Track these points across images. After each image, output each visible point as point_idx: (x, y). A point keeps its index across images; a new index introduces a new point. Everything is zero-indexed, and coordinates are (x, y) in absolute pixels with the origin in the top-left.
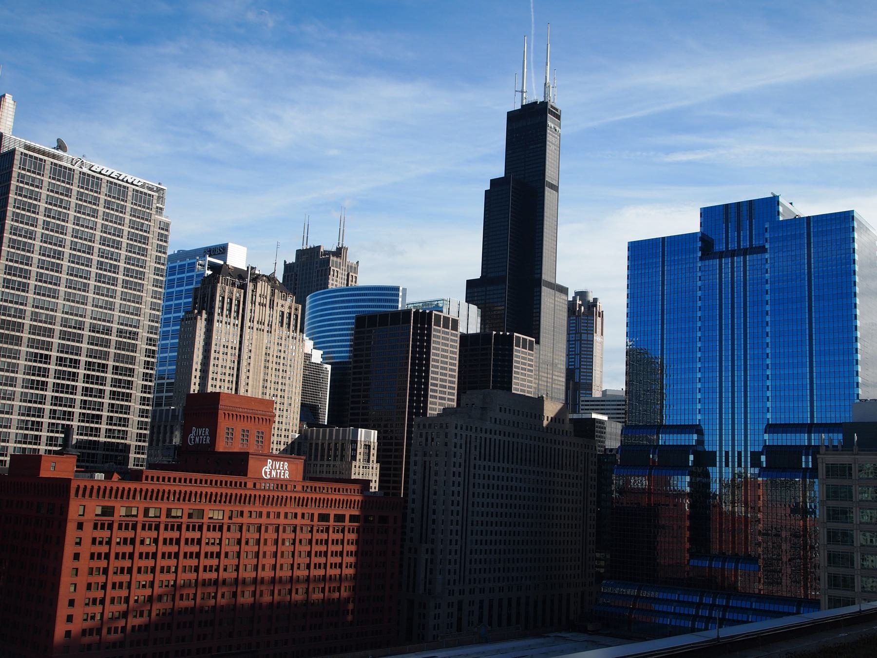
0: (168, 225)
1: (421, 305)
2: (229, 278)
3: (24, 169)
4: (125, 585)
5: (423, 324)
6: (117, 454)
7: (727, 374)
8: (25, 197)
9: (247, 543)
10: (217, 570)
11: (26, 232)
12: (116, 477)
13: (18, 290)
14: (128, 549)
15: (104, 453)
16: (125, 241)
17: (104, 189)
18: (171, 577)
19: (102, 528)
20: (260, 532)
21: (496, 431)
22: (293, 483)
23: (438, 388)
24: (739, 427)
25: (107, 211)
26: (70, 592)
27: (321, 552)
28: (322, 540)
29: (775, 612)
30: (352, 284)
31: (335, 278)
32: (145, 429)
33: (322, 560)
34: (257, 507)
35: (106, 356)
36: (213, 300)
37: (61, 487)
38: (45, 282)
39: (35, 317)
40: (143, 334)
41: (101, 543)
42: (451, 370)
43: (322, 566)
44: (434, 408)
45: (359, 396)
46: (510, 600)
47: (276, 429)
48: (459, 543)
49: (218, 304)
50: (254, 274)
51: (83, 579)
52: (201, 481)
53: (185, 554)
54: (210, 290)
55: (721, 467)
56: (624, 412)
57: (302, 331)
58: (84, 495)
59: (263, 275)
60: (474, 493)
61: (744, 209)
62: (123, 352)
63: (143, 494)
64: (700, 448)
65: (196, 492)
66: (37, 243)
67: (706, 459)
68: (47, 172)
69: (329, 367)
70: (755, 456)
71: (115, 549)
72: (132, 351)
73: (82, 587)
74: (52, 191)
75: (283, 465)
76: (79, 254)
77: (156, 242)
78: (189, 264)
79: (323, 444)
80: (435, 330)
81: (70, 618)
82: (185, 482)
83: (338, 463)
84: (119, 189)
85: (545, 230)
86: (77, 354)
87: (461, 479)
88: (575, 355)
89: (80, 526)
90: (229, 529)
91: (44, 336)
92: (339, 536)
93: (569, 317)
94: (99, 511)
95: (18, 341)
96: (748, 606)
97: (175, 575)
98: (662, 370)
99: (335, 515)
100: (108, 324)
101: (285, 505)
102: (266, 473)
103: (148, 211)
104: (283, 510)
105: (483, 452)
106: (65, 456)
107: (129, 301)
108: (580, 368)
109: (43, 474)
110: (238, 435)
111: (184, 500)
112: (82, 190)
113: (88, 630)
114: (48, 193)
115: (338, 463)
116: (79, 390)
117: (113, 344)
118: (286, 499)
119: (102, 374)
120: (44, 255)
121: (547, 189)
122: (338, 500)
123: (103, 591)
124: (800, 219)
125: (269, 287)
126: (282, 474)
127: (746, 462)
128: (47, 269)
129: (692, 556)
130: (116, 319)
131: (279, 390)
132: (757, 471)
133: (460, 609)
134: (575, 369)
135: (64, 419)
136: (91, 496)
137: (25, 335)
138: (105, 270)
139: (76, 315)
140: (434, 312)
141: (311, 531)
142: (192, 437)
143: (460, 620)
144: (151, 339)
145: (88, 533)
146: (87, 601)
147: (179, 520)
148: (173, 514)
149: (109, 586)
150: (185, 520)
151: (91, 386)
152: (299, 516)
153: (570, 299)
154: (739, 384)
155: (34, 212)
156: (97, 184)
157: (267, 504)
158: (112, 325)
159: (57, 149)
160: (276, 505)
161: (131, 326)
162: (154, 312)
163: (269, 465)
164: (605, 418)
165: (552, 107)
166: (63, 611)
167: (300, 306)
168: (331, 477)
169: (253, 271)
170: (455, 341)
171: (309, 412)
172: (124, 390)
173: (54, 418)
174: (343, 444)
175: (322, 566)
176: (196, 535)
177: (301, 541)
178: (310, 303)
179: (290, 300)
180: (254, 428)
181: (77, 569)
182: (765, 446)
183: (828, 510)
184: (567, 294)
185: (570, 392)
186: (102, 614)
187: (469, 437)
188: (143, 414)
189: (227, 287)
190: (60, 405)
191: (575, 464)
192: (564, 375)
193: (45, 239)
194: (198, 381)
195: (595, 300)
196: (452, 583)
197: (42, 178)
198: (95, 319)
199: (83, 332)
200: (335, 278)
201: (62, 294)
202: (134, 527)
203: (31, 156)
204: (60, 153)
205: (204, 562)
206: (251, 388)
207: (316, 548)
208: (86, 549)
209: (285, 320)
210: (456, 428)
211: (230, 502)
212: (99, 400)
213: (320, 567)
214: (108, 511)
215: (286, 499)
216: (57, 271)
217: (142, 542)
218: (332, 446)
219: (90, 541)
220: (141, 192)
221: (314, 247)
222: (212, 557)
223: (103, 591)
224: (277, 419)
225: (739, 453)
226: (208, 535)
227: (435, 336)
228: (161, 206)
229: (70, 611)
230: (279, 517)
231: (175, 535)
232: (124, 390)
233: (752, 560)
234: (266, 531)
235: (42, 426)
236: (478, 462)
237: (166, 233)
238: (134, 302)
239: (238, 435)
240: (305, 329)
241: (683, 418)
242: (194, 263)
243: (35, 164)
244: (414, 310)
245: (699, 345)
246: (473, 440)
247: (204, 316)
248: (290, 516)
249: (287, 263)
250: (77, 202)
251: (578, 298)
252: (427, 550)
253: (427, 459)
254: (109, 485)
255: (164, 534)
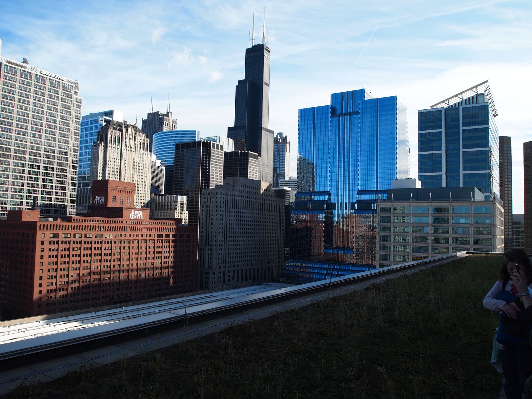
0: (80, 100)
1: (206, 139)
2: (114, 126)
3: (6, 73)
4: (66, 269)
5: (207, 147)
6: (61, 209)
7: (341, 169)
8: (8, 86)
9: (124, 248)
10: (110, 261)
11: (9, 104)
12: (59, 220)
13: (7, 132)
14: (67, 253)
15: (54, 209)
16: (59, 108)
17: (48, 83)
18: (89, 265)
19: (54, 243)
20: (130, 243)
21: (239, 196)
22: (145, 221)
23: (214, 177)
24: (346, 192)
25: (50, 93)
26: (40, 273)
27: (159, 252)
28: (159, 246)
29: (355, 270)
30: (174, 129)
31: (166, 126)
32: (74, 197)
33: (160, 255)
34: (128, 232)
35: (53, 163)
36: (107, 137)
37: (32, 225)
38: (21, 128)
39: (16, 145)
40: (71, 153)
41: (53, 250)
42: (220, 168)
43: (160, 258)
44: (212, 186)
45: (178, 181)
46: (246, 269)
47: (136, 196)
48: (223, 246)
49: (109, 139)
50: (126, 124)
51: (46, 267)
52: (100, 221)
53: (95, 254)
54: (105, 132)
55: (338, 210)
56: (296, 186)
57: (151, 151)
58: (44, 229)
59: (130, 125)
60: (229, 224)
61: (350, 94)
62: (61, 161)
63: (73, 227)
64: (329, 202)
65: (98, 226)
66: (15, 109)
67: (332, 206)
68: (18, 74)
69: (164, 168)
70: (353, 205)
71: (60, 253)
72: (66, 161)
73: (45, 271)
74: (21, 84)
75: (140, 213)
76: (37, 114)
77: (75, 108)
78: (95, 120)
79: (161, 203)
80: (213, 150)
81: (41, 285)
82: (93, 221)
83: (169, 211)
84: (55, 83)
85: (263, 104)
86: (38, 163)
87: (224, 218)
88: (277, 161)
89: (43, 243)
90: (115, 242)
91: (21, 154)
92: (160, 244)
93: (274, 144)
94: (51, 236)
95: (9, 156)
96: (348, 269)
97: (90, 264)
98: (313, 168)
99: (165, 235)
100: (53, 148)
101: (141, 231)
102: (131, 216)
103: (70, 93)
104: (140, 233)
105: (233, 205)
106: (34, 211)
107: (63, 137)
108: (279, 167)
109: (23, 219)
110: (118, 199)
111: (93, 230)
112: (37, 83)
113: (53, 290)
114: (19, 84)
115: (169, 211)
116: (41, 180)
117: (56, 157)
118: (142, 228)
119: (52, 172)
120: (19, 115)
121: (264, 85)
122: (157, 228)
123: (56, 272)
124: (374, 99)
125: (134, 130)
126: (139, 217)
127: (349, 207)
128: (21, 122)
129: (325, 248)
130: (57, 145)
131: (140, 179)
132: (353, 211)
133: (224, 274)
134: (277, 167)
135: (34, 193)
136: (47, 229)
137: (12, 154)
138: (50, 122)
139: (37, 144)
140: (212, 142)
141: (154, 242)
142: (96, 201)
143: (224, 279)
144: (75, 155)
145: (47, 246)
146: (48, 277)
147: (91, 239)
148: (88, 236)
149: (59, 270)
150: (94, 239)
151: (46, 178)
152: (148, 236)
153: (275, 136)
154: (346, 173)
155: (13, 94)
156: (44, 80)
157: (133, 231)
158: (55, 148)
159: (24, 63)
160: (137, 231)
161: (64, 149)
162: (75, 142)
163: (97, 199)
164: (290, 189)
165: (266, 47)
166: (37, 282)
167: (149, 139)
168: (166, 218)
169: (125, 123)
170: (222, 155)
171: (155, 189)
172: (62, 179)
173: (29, 193)
174: (171, 203)
175: (160, 258)
176: (99, 245)
177: (149, 247)
178: (154, 138)
179: (144, 136)
180: (125, 196)
181: (43, 263)
182: (357, 200)
183: (380, 227)
184: (273, 134)
185: (275, 178)
186: (56, 283)
187: (227, 198)
188: (73, 190)
189: (113, 131)
190: (32, 187)
191: (275, 210)
192: (272, 171)
193: (19, 107)
194: (101, 175)
195: (286, 136)
196: (220, 263)
197: (16, 77)
198: (46, 146)
199: (54, 154)
200: (166, 126)
201: (29, 134)
202: (69, 243)
203: (10, 66)
204: (25, 65)
205: (104, 258)
206: (127, 178)
207: (157, 250)
208: (46, 254)
209: (142, 146)
210: (221, 194)
211: (115, 230)
212: (51, 184)
213: (159, 258)
214: (56, 236)
215: (142, 228)
216: (26, 123)
217: (73, 249)
218: (166, 204)
219: (48, 249)
220: (66, 84)
221: (156, 112)
222: (107, 255)
223: (56, 272)
224: (136, 192)
225: (346, 203)
226: (105, 245)
227: (212, 153)
228: (77, 91)
229: (41, 282)
230: (139, 236)
231: (89, 246)
232: (62, 179)
233: (350, 249)
234: (133, 243)
235: (23, 197)
236: (231, 210)
237: (80, 104)
238: (65, 137)
239: (118, 199)
240: (153, 150)
241: (324, 188)
242: (98, 119)
243: (12, 70)
244: (202, 141)
245: (329, 156)
246: (229, 199)
247: (103, 144)
248: (144, 236)
249: (144, 119)
250: (34, 89)
251: (279, 135)
252: (209, 249)
253: (208, 209)
254: (56, 223)
255: (84, 246)
